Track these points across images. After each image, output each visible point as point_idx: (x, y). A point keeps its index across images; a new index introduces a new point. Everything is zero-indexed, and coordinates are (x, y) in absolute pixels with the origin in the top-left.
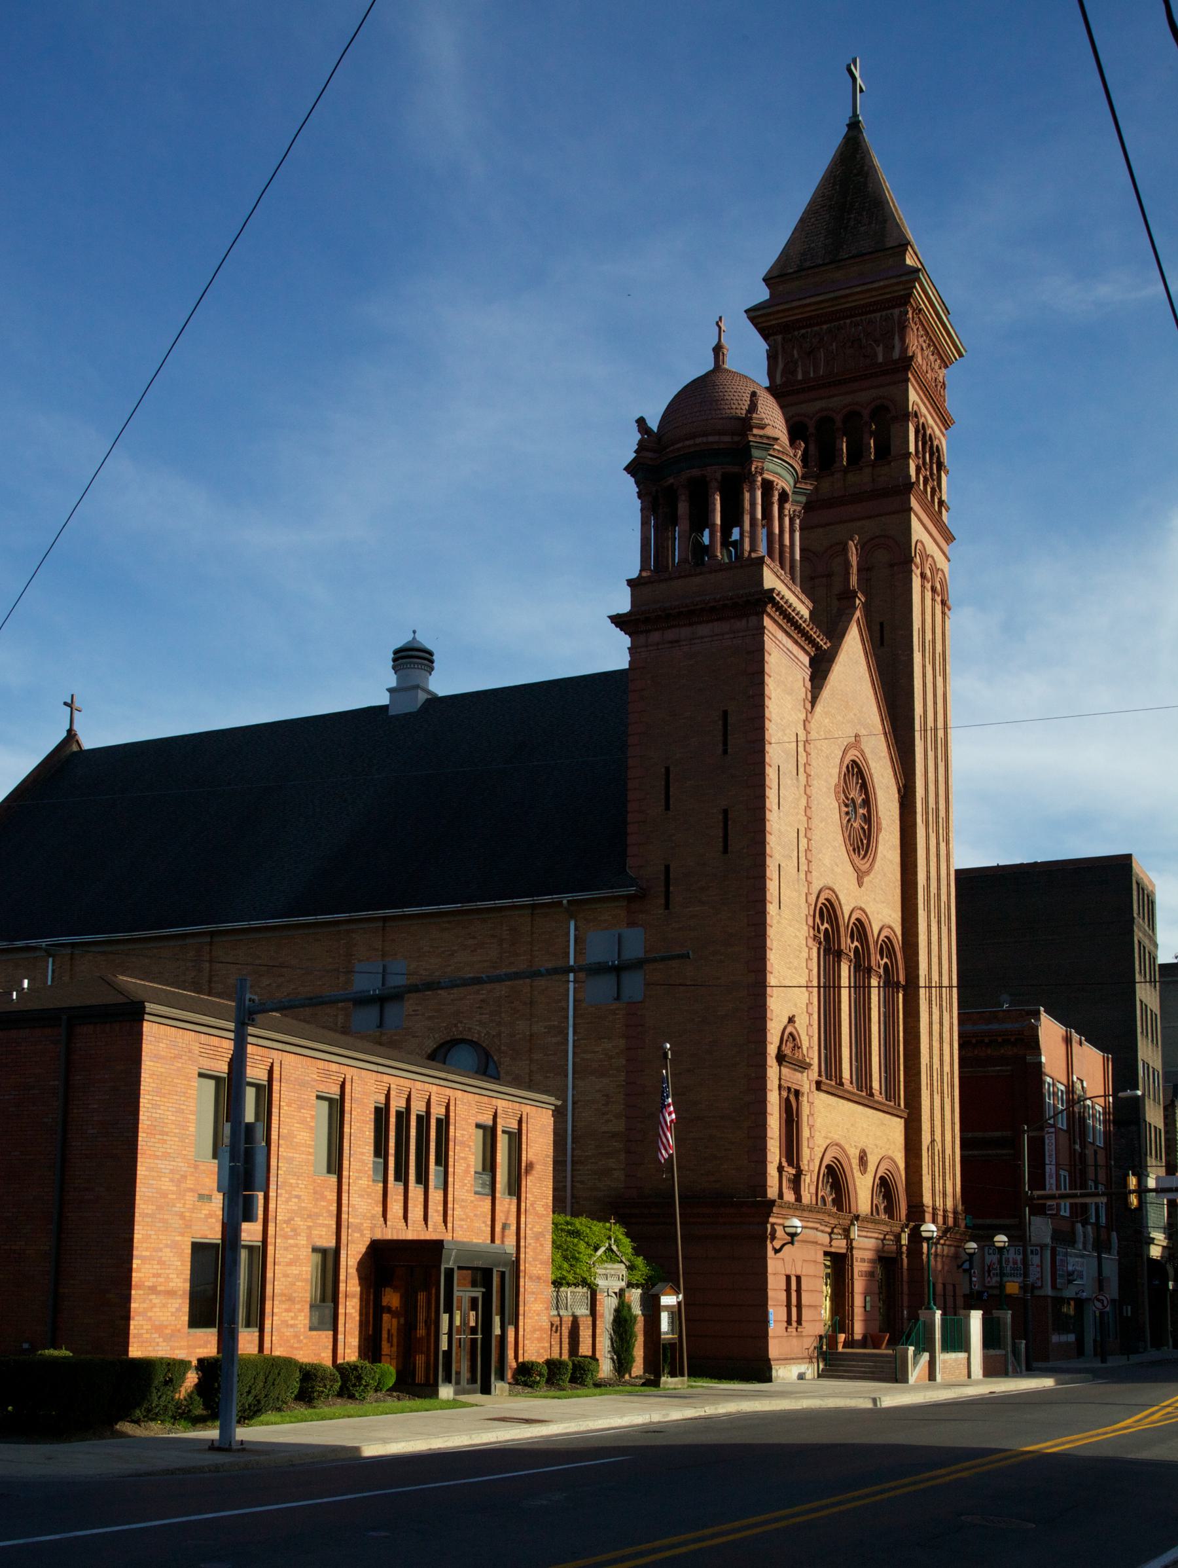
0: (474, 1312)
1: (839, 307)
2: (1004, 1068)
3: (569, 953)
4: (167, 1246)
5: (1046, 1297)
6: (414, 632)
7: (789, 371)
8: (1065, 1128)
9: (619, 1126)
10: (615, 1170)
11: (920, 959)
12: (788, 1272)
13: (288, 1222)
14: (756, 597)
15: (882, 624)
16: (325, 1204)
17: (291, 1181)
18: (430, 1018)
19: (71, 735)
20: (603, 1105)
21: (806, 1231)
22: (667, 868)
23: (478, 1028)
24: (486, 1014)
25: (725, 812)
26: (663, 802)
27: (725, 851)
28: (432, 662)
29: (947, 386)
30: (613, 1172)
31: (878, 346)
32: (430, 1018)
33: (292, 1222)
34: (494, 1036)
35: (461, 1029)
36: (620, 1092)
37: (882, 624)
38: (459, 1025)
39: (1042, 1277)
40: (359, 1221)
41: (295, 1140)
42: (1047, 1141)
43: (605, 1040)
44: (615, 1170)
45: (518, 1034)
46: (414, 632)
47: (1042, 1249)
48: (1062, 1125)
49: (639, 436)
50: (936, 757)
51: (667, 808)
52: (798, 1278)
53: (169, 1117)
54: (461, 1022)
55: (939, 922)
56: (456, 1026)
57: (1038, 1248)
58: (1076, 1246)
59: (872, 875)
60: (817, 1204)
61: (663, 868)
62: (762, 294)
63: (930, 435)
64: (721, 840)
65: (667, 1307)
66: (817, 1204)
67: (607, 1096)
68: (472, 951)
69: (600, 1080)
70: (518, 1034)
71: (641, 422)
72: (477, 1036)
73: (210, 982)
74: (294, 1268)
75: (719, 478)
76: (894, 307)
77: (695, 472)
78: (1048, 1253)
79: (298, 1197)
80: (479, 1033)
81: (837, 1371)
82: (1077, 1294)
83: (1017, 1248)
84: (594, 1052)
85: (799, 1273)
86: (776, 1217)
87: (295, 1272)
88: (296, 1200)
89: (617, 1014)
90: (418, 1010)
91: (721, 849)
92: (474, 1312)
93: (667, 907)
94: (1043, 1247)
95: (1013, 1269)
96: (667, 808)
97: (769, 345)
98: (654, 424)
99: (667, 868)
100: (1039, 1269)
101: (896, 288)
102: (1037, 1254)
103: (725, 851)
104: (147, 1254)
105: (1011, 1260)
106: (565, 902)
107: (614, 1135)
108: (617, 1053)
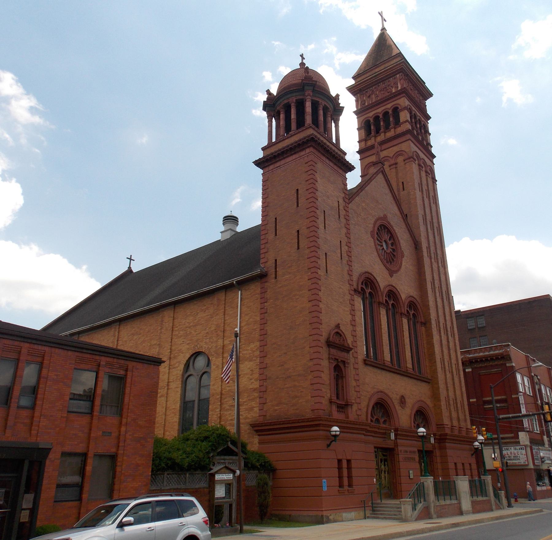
1: (377, 79)
2: (498, 370)
3: (238, 306)
5: (531, 469)
6: (231, 211)
7: (363, 103)
8: (531, 395)
9: (256, 385)
10: (255, 407)
12: (340, 458)
14: (306, 139)
15: (403, 182)
18: (188, 344)
19: (130, 268)
20: (250, 375)
21: (342, 434)
22: (276, 260)
23: (205, 346)
24: (208, 339)
25: (298, 231)
26: (274, 233)
27: (298, 248)
28: (238, 222)
30: (254, 408)
31: (393, 88)
32: (188, 344)
34: (210, 348)
35: (199, 347)
36: (257, 368)
37: (403, 182)
38: (198, 345)
39: (527, 460)
42: (520, 399)
43: (252, 344)
44: (255, 407)
45: (219, 346)
46: (231, 211)
47: (525, 447)
48: (530, 393)
49: (267, 96)
50: (434, 233)
51: (276, 235)
52: (349, 461)
54: (199, 344)
55: (442, 299)
56: (197, 346)
57: (524, 447)
58: (545, 446)
59: (399, 273)
61: (274, 261)
62: (353, 82)
63: (419, 119)
64: (296, 244)
65: (221, 482)
67: (252, 370)
68: (204, 312)
69: (250, 363)
70: (219, 346)
71: (268, 92)
72: (204, 349)
73: (118, 341)
75: (295, 101)
76: (397, 74)
77: (286, 102)
78: (529, 449)
80: (205, 347)
81: (376, 514)
82: (548, 467)
83: (515, 447)
84: (247, 350)
85: (349, 458)
86: (322, 426)
89: (257, 331)
90: (184, 341)
91: (297, 248)
93: (276, 278)
94: (526, 446)
95: (514, 457)
96: (276, 235)
97: (355, 98)
98: (274, 91)
99: (276, 260)
100: (526, 456)
101: (397, 67)
102: (523, 449)
103: (298, 248)
105: (513, 453)
106: (234, 282)
107: (255, 390)
108: (256, 349)
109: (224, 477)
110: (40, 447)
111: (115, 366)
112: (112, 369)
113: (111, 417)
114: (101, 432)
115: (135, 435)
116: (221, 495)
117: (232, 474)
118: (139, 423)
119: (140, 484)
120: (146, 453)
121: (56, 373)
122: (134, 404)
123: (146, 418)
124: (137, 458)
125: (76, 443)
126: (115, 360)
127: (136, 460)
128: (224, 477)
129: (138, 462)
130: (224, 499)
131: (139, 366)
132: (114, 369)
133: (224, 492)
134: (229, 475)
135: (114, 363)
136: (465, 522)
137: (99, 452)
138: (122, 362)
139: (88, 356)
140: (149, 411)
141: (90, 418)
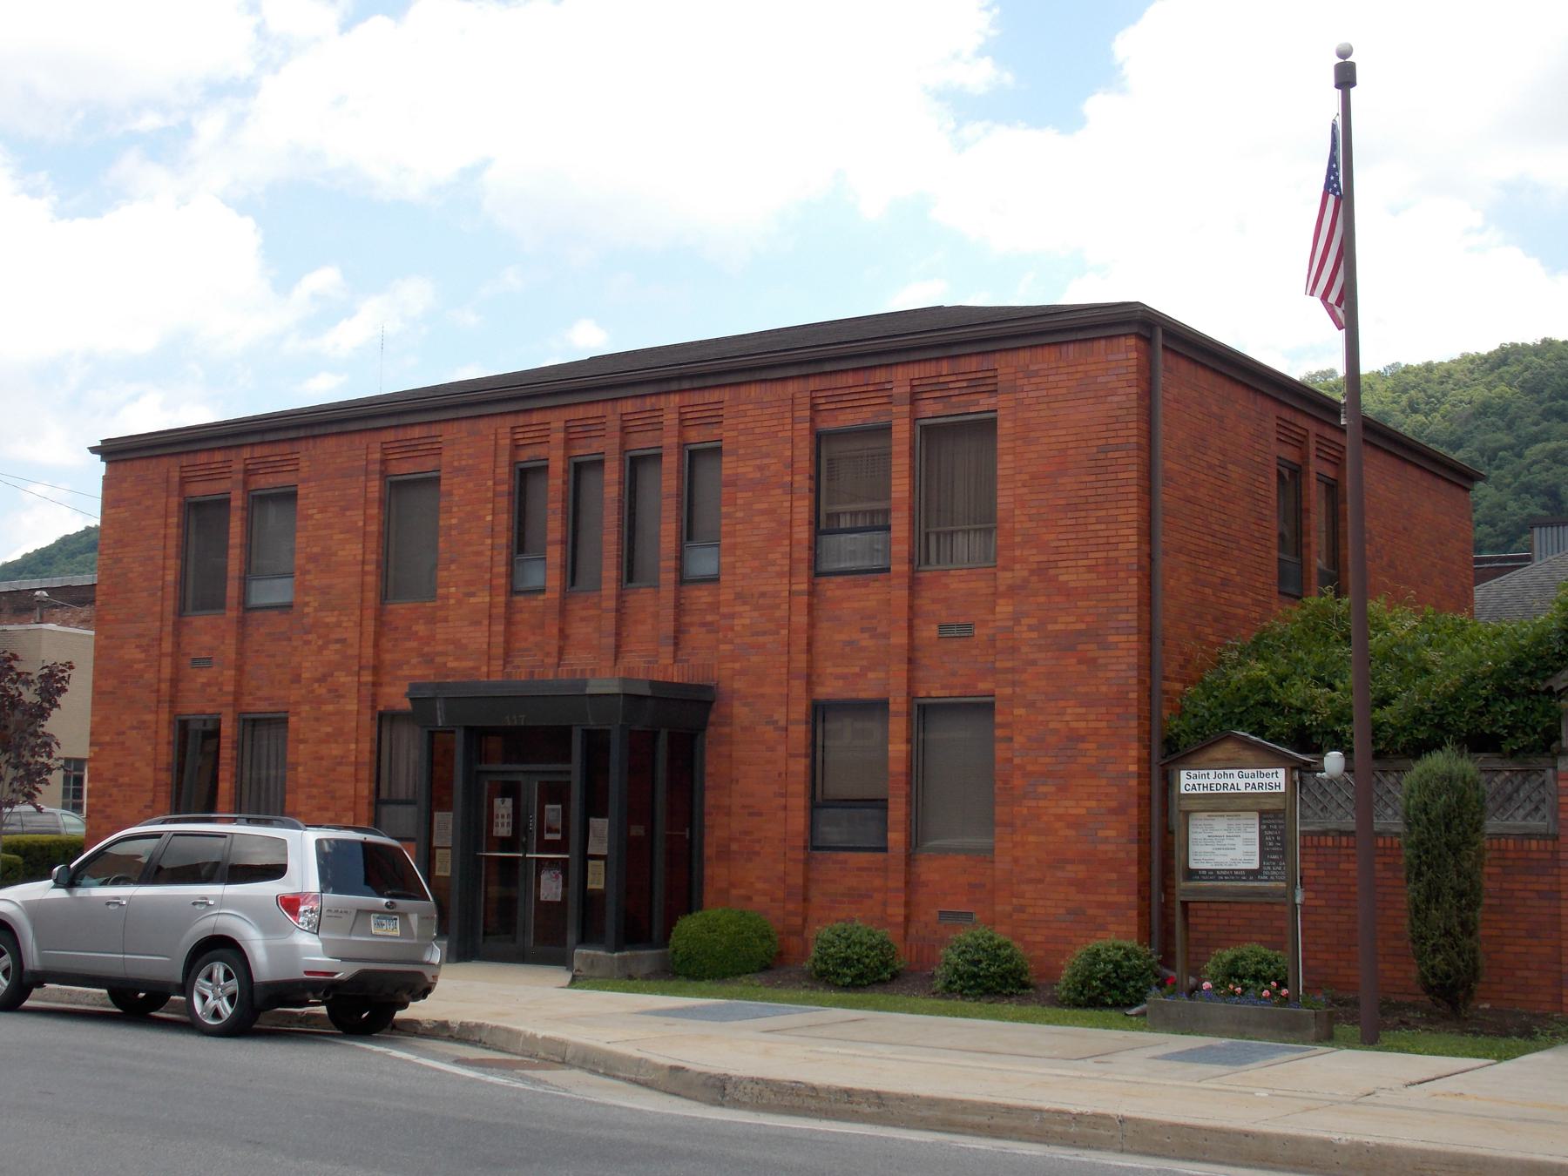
0: (509, 802)
4: (133, 728)
11: (52, 542)
13: (322, 679)
16: (414, 644)
17: (327, 620)
29: (1330, 78)
33: (329, 679)
40: (471, 664)
41: (334, 559)
46: (1346, 77)
53: (1124, 398)
60: (7, 833)
66: (7, 833)
74: (333, 746)
79: (342, 641)
87: (335, 752)
88: (338, 646)
92: (509, 802)
104: (107, 739)
109: (1236, 780)
110: (589, 691)
111: (951, 386)
112: (945, 400)
113: (965, 572)
114: (935, 627)
115: (1050, 627)
116: (1234, 861)
117: (1282, 772)
118: (1062, 578)
119: (1093, 804)
120: (1104, 689)
121: (758, 462)
122: (1034, 511)
123: (1091, 555)
124: (1069, 711)
125: (857, 670)
126: (945, 367)
127: (1067, 718)
128: (1236, 780)
129: (1074, 725)
130: (1256, 879)
131: (1041, 360)
132: (954, 399)
133: (1256, 848)
134: (1262, 775)
135: (942, 380)
136: (739, 1082)
137: (933, 694)
138: (972, 364)
139: (849, 380)
140: (1103, 526)
141: (627, 605)
